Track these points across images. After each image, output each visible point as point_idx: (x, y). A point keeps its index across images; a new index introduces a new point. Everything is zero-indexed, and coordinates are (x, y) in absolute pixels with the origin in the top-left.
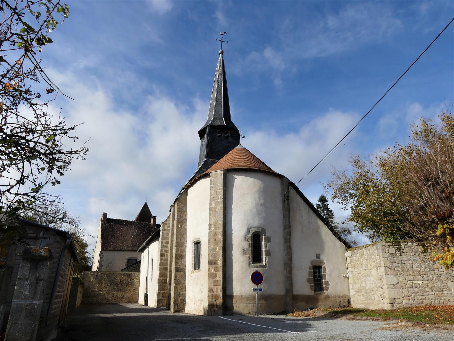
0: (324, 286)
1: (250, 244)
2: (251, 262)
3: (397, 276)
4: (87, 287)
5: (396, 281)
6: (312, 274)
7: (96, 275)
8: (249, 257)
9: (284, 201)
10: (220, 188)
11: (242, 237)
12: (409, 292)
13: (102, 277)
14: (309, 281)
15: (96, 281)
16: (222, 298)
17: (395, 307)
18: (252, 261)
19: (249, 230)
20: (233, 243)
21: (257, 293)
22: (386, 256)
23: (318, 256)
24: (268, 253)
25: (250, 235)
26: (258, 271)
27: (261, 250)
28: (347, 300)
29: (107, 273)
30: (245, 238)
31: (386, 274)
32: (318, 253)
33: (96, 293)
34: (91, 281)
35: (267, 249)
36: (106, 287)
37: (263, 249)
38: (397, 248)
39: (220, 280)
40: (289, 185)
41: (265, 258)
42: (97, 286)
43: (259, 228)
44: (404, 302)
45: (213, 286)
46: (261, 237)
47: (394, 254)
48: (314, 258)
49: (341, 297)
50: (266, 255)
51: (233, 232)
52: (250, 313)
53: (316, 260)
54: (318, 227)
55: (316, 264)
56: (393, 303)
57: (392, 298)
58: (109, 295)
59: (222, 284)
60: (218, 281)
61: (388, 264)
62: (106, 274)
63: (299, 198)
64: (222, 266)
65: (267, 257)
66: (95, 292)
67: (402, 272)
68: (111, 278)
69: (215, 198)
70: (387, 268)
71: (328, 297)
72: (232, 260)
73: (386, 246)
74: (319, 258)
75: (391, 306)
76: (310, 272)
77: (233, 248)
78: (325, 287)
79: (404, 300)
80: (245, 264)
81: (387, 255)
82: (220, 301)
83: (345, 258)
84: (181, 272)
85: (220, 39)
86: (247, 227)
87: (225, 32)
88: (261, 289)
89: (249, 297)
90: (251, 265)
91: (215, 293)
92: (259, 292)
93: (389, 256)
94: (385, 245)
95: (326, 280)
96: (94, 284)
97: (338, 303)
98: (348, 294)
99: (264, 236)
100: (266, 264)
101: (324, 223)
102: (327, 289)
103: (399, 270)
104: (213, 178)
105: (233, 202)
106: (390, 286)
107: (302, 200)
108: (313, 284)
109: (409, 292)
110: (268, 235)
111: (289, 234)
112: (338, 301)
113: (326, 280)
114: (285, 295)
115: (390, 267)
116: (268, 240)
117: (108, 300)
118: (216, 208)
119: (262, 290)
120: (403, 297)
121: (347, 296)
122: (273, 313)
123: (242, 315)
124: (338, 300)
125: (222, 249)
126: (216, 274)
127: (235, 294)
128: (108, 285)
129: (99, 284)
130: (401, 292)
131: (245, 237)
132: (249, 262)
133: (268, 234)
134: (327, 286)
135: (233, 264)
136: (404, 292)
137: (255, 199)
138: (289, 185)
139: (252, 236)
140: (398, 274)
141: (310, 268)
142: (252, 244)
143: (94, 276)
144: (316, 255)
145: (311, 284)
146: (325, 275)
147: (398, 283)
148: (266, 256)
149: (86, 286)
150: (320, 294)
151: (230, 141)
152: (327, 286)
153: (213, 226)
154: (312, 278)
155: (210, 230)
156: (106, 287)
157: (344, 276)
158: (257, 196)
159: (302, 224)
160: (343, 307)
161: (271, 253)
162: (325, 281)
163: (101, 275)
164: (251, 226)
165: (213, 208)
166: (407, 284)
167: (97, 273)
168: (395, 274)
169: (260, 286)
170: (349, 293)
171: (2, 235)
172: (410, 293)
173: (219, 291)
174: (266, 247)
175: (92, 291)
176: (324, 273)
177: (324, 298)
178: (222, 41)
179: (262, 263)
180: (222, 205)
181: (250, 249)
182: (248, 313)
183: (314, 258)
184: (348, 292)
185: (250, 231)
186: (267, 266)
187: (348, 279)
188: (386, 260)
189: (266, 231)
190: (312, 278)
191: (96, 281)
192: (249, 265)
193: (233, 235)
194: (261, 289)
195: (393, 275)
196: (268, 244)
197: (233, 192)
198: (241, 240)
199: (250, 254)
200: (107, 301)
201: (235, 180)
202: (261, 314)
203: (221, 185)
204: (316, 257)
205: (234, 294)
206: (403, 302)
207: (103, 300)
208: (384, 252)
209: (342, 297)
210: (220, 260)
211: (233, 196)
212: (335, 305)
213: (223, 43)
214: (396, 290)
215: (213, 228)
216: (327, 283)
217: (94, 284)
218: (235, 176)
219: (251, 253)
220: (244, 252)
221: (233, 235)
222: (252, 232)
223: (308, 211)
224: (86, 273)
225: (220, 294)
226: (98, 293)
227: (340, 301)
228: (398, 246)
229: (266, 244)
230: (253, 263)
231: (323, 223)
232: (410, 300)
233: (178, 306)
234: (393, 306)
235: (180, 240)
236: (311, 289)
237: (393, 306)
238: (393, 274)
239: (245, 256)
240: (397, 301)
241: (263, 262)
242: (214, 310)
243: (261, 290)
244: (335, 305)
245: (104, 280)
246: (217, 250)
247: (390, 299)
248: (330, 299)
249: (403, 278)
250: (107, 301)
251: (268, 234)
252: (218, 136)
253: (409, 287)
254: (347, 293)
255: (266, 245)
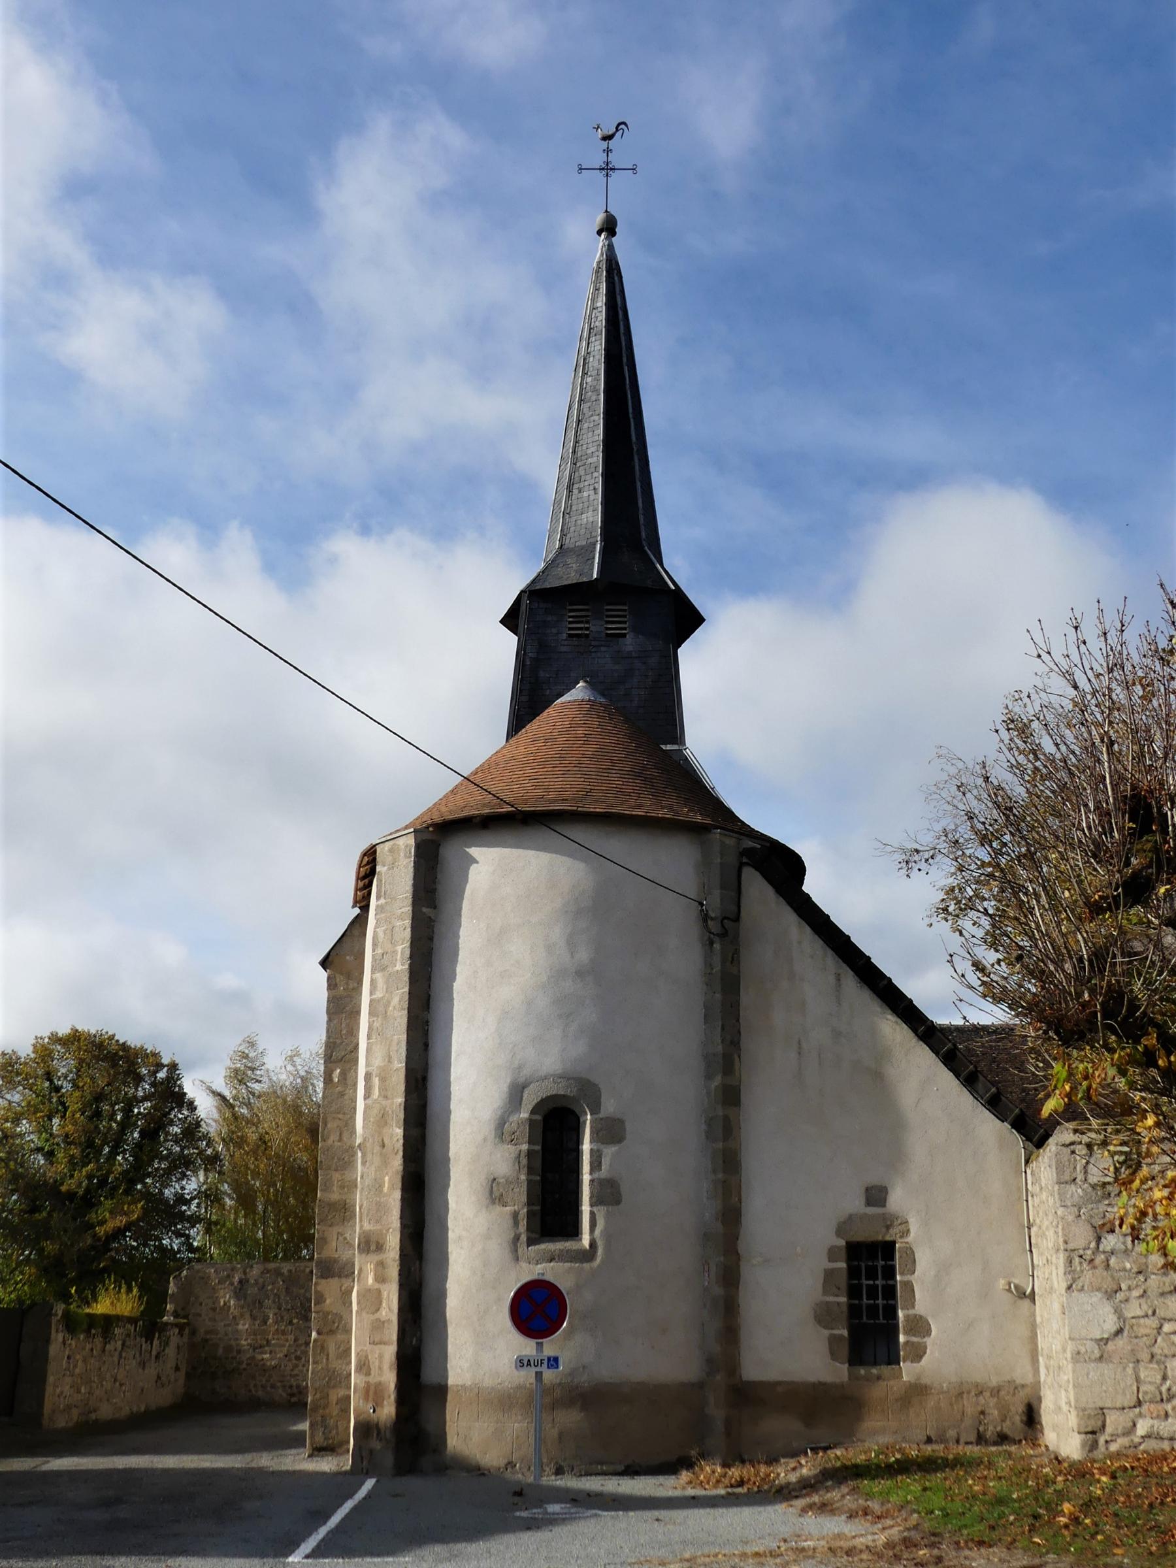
0: (902, 1338)
1: (523, 1155)
2: (524, 1238)
3: (1120, 1296)
4: (207, 1332)
5: (1111, 1325)
6: (843, 1281)
7: (241, 1282)
8: (515, 1216)
9: (711, 943)
10: (403, 910)
11: (488, 1130)
12: (1164, 1378)
13: (263, 1286)
14: (823, 1316)
15: (242, 1307)
16: (393, 1397)
17: (508, 1474)
18: (529, 1229)
19: (516, 1092)
20: (452, 1154)
21: (539, 1375)
22: (1076, 1198)
23: (876, 1196)
24: (608, 1193)
25: (524, 1115)
26: (549, 1277)
27: (580, 1177)
28: (1021, 1408)
29: (285, 1271)
30: (501, 1131)
31: (1069, 1288)
32: (873, 1179)
33: (245, 1357)
34: (222, 1308)
35: (604, 1173)
36: (283, 1333)
37: (586, 1178)
38: (1122, 1158)
39: (389, 1321)
40: (745, 860)
41: (592, 1214)
42: (244, 1326)
43: (563, 1083)
44: (1142, 1429)
45: (368, 1347)
46: (581, 1120)
47: (1109, 1188)
48: (855, 1204)
49: (987, 1394)
50: (596, 1201)
51: (452, 1107)
52: (510, 1464)
53: (863, 1217)
54: (882, 1055)
55: (863, 1234)
56: (1093, 1433)
57: (1092, 1405)
58: (296, 1366)
59: (395, 1337)
60: (383, 1322)
61: (1082, 1236)
62: (282, 1274)
63: (790, 919)
64: (397, 1257)
65: (601, 1212)
66: (239, 1352)
67: (1141, 1278)
68: (302, 1291)
69: (385, 961)
70: (1077, 1260)
71: (919, 1391)
72: (447, 1229)
73: (1078, 1148)
74: (884, 1206)
75: (1083, 1445)
76: (829, 1275)
77: (452, 1174)
78: (907, 1343)
79: (1140, 1415)
80: (497, 1249)
81: (1080, 1191)
82: (388, 1410)
83: (1020, 1198)
84: (343, 1280)
85: (599, 160)
86: (509, 1080)
87: (619, 124)
88: (556, 1359)
89: (509, 1396)
90: (522, 1248)
91: (373, 1379)
92: (549, 1375)
93: (1086, 1200)
94: (1072, 1143)
95: (911, 1312)
96: (234, 1317)
97: (968, 1422)
98: (1029, 1379)
99: (589, 1117)
100: (593, 1244)
101: (915, 1031)
102: (918, 1353)
103: (1128, 1266)
104: (386, 868)
105: (458, 969)
106: (1083, 1350)
107: (808, 929)
108: (845, 1333)
109: (1164, 1378)
110: (611, 1110)
111: (731, 1096)
112: (970, 1410)
113: (911, 1312)
114: (701, 1385)
115: (1089, 1252)
116: (611, 1132)
117: (295, 1390)
118: (389, 1002)
119: (561, 1362)
120: (1139, 1403)
121: (1023, 1386)
122: (621, 1468)
123: (477, 1471)
124: (970, 1407)
125: (400, 1185)
126: (379, 1292)
127: (452, 1380)
128: (291, 1323)
129: (253, 1318)
130: (1130, 1380)
131: (501, 1124)
132: (516, 1239)
133: (609, 1107)
134: (915, 1339)
135: (451, 1247)
136: (1142, 1376)
137: (550, 948)
138: (745, 860)
139: (538, 1117)
140: (1124, 1287)
141: (832, 1254)
142: (530, 1154)
143: (232, 1284)
144: (867, 1190)
145: (836, 1332)
146: (909, 1287)
147: (1119, 1332)
148: (595, 1209)
149: (202, 1330)
150: (879, 1378)
151: (630, 648)
152: (915, 1339)
153: (376, 1081)
154: (843, 1299)
155: (367, 1101)
156: (283, 1333)
157: (1009, 1290)
158: (558, 934)
159: (799, 1043)
160: (995, 1444)
161: (625, 1190)
162: (907, 1317)
163: (261, 1280)
164: (526, 1072)
165: (379, 1001)
166: (1159, 1340)
167: (245, 1273)
168: (1108, 1284)
169: (550, 1347)
170: (1036, 1371)
171: (1107, 917)
172: (1168, 1383)
173: (386, 1366)
174: (596, 1165)
175: (228, 1349)
176: (906, 1278)
177: (897, 1400)
178: (607, 169)
179: (581, 1239)
180: (407, 989)
181: (523, 1177)
182: (502, 1465)
183: (855, 1204)
184: (1029, 1368)
185: (525, 1096)
186: (600, 1252)
187: (1033, 1301)
188: (1070, 1218)
189: (603, 1091)
190: (838, 1304)
191: (242, 1307)
192: (515, 1250)
193: (454, 1118)
194: (556, 1359)
195: (1099, 1295)
196: (609, 1152)
197: (460, 926)
198: (485, 1140)
199: (519, 1199)
200: (292, 1395)
201: (473, 869)
202: (559, 1471)
203: (406, 897)
204: (863, 1200)
205: (451, 1381)
206: (1138, 1426)
207: (273, 1386)
208: (1067, 1177)
209: (996, 1391)
210: (394, 1230)
211: (458, 944)
212: (952, 1433)
213: (615, 175)
214: (1111, 1366)
215: (376, 1093)
216: (920, 1326)
217: (234, 1317)
218: (474, 851)
219: (524, 1199)
220: (494, 1194)
221: (453, 1117)
222: (531, 1098)
223: (832, 979)
224: (198, 1271)
225: (389, 1378)
226: (253, 1358)
227: (983, 1413)
228: (1126, 1149)
229: (598, 1151)
230: (531, 1242)
231: (910, 1034)
232: (1167, 1415)
233: (326, 1427)
234: (1094, 1446)
235: (340, 1140)
236: (833, 1355)
237: (1094, 1446)
238: (1099, 1290)
239: (498, 1209)
240: (1115, 1421)
241: (582, 1234)
242: (371, 1452)
243: (553, 1362)
244: (952, 1433)
245: (274, 1302)
246: (385, 1189)
247: (1082, 1410)
248: (931, 1403)
249: (1145, 1307)
250: (292, 1395)
251: (609, 1107)
252: (570, 636)
253: (1166, 1351)
254: (1022, 1373)
255: (600, 1156)
